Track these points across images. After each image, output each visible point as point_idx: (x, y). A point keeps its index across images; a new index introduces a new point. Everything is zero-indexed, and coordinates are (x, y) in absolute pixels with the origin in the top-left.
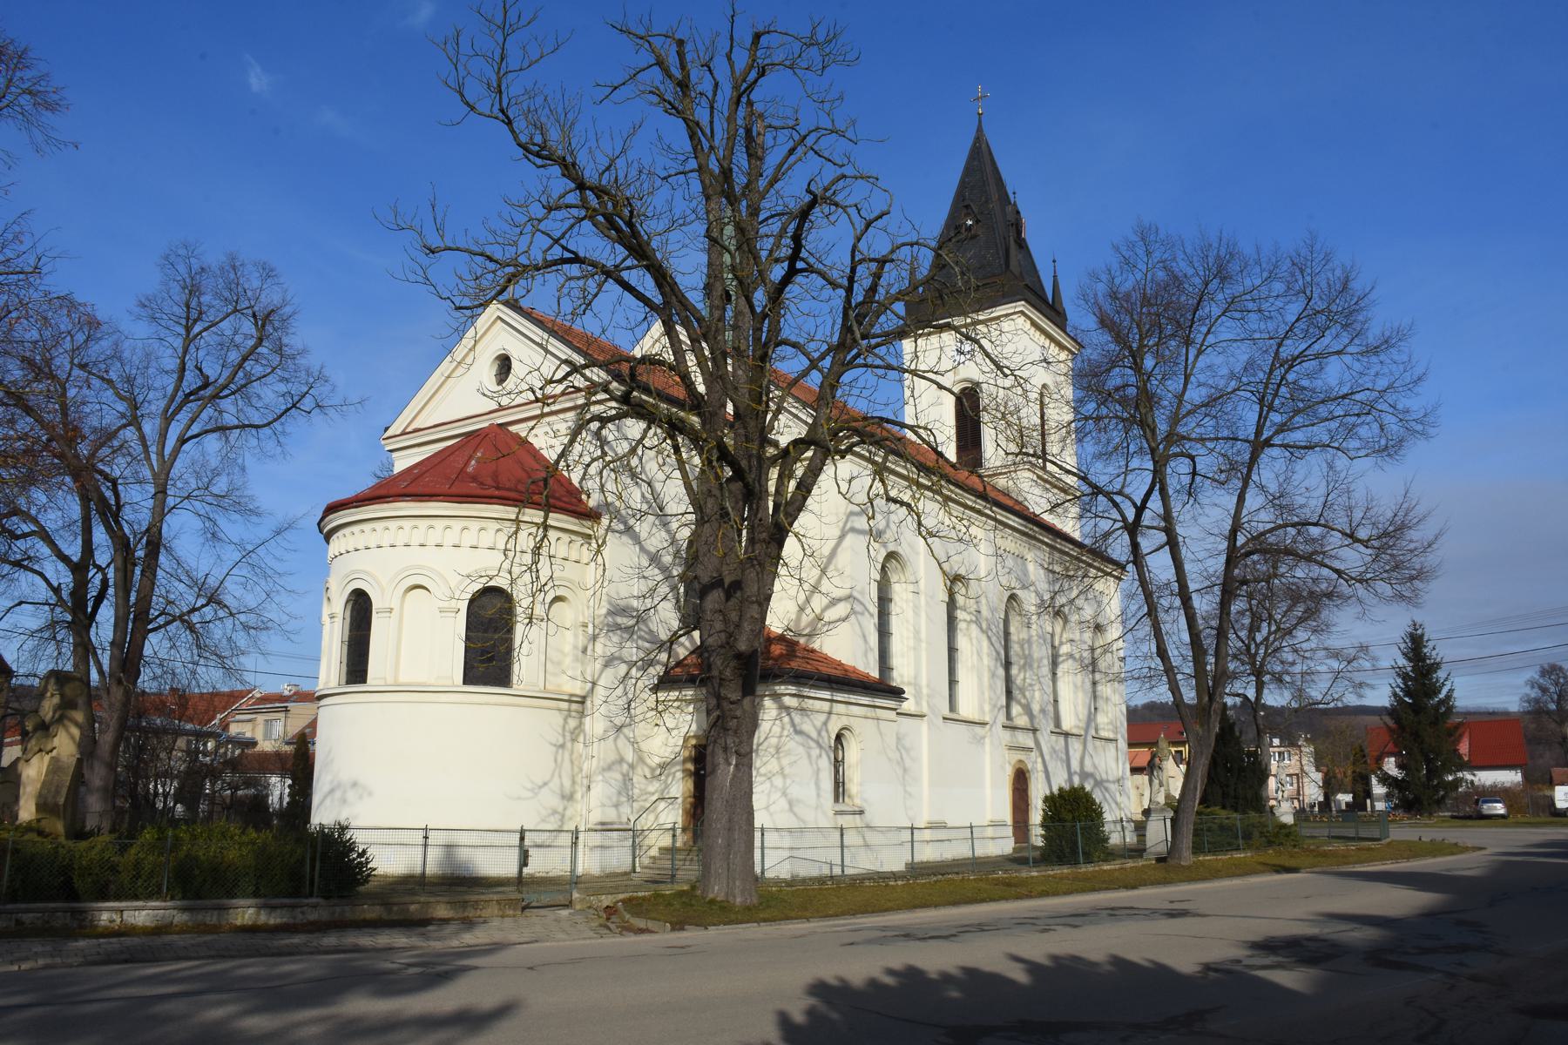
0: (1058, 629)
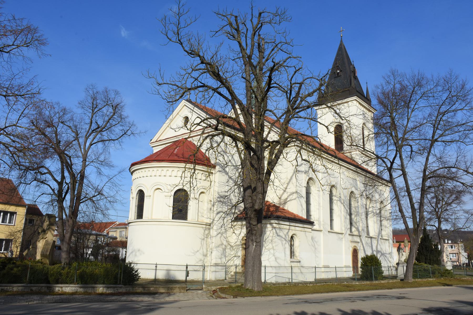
0: (368, 203)
